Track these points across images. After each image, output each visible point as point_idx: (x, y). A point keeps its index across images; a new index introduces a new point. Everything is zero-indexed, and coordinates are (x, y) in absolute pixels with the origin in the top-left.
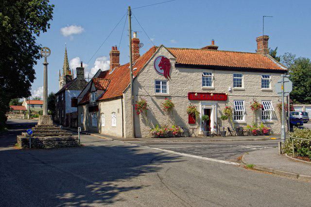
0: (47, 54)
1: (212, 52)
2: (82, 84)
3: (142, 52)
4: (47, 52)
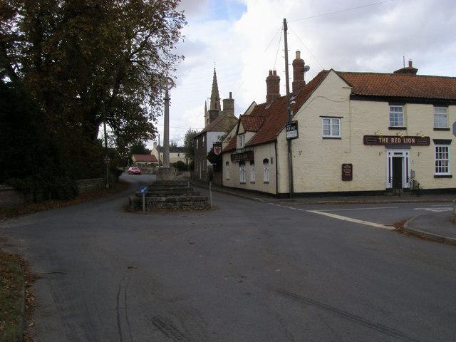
1: (406, 77)
3: (308, 77)
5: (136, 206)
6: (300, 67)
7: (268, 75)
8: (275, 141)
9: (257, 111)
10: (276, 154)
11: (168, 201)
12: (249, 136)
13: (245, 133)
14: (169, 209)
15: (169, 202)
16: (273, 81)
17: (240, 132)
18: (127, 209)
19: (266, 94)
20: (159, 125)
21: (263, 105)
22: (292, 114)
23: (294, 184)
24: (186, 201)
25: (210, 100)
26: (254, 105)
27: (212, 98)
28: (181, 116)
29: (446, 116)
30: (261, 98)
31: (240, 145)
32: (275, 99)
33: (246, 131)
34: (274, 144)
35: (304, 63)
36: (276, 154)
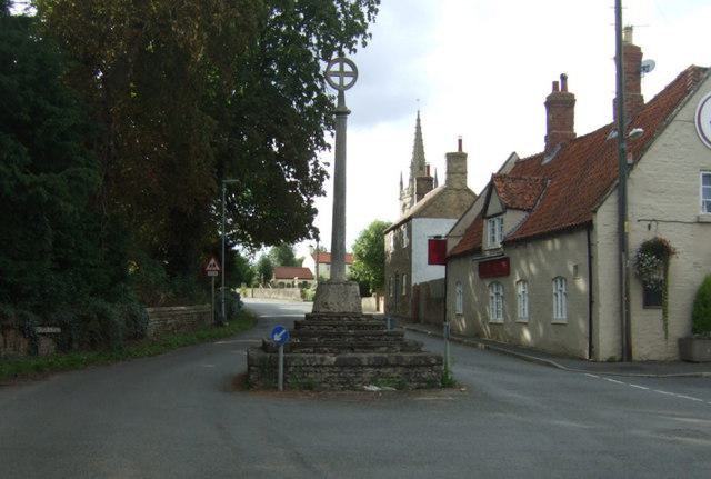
0: (348, 80)
2: (461, 200)
4: (348, 74)
5: (260, 376)
6: (630, 63)
7: (549, 91)
8: (589, 227)
9: (517, 177)
10: (591, 258)
11: (341, 364)
12: (513, 221)
13: (505, 212)
14: (348, 384)
15: (342, 367)
16: (560, 105)
17: (491, 211)
18: (243, 383)
19: (545, 133)
20: (323, 221)
21: (539, 158)
22: (630, 161)
23: (633, 327)
24: (387, 365)
25: (409, 170)
26: (514, 159)
27: (412, 167)
28: (367, 185)
29: (219, 323)
30: (532, 142)
31: (492, 240)
32: (564, 141)
33: (506, 208)
34: (583, 235)
35: (640, 55)
36: (591, 258)
